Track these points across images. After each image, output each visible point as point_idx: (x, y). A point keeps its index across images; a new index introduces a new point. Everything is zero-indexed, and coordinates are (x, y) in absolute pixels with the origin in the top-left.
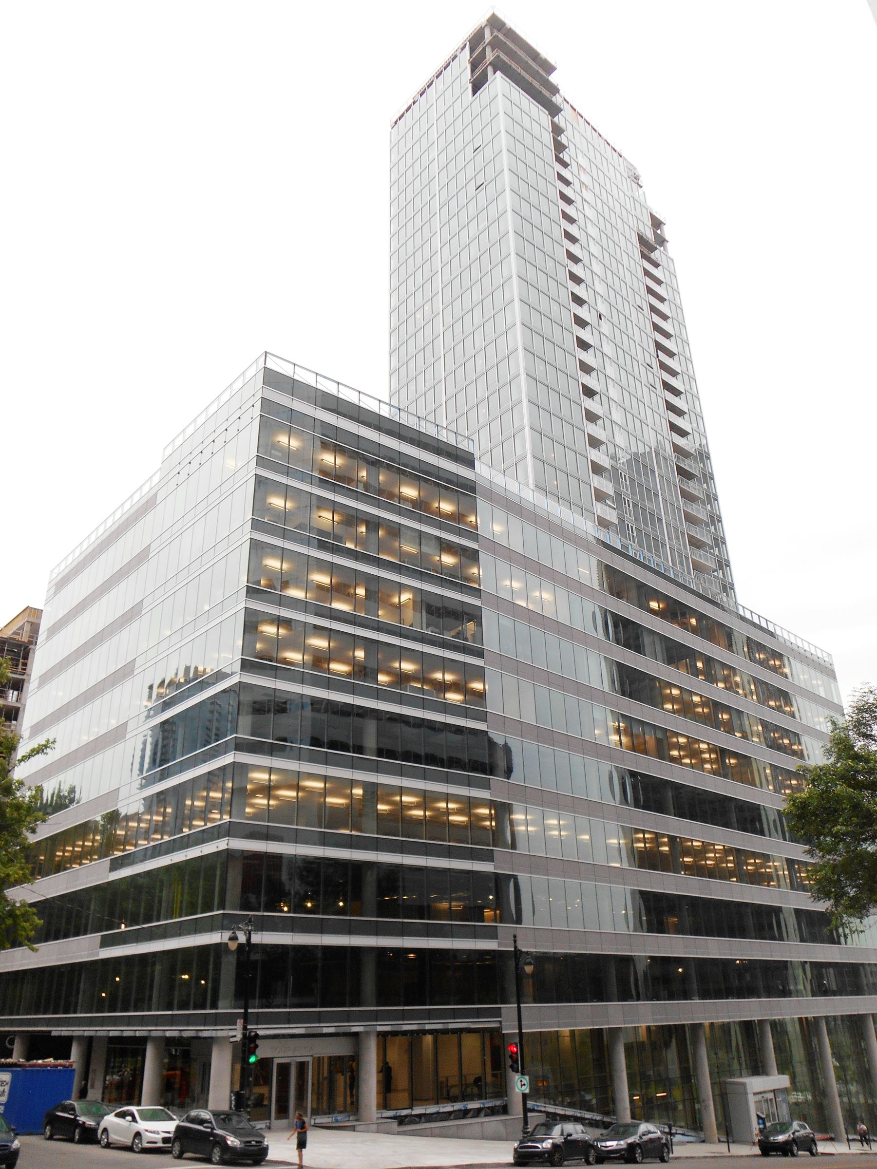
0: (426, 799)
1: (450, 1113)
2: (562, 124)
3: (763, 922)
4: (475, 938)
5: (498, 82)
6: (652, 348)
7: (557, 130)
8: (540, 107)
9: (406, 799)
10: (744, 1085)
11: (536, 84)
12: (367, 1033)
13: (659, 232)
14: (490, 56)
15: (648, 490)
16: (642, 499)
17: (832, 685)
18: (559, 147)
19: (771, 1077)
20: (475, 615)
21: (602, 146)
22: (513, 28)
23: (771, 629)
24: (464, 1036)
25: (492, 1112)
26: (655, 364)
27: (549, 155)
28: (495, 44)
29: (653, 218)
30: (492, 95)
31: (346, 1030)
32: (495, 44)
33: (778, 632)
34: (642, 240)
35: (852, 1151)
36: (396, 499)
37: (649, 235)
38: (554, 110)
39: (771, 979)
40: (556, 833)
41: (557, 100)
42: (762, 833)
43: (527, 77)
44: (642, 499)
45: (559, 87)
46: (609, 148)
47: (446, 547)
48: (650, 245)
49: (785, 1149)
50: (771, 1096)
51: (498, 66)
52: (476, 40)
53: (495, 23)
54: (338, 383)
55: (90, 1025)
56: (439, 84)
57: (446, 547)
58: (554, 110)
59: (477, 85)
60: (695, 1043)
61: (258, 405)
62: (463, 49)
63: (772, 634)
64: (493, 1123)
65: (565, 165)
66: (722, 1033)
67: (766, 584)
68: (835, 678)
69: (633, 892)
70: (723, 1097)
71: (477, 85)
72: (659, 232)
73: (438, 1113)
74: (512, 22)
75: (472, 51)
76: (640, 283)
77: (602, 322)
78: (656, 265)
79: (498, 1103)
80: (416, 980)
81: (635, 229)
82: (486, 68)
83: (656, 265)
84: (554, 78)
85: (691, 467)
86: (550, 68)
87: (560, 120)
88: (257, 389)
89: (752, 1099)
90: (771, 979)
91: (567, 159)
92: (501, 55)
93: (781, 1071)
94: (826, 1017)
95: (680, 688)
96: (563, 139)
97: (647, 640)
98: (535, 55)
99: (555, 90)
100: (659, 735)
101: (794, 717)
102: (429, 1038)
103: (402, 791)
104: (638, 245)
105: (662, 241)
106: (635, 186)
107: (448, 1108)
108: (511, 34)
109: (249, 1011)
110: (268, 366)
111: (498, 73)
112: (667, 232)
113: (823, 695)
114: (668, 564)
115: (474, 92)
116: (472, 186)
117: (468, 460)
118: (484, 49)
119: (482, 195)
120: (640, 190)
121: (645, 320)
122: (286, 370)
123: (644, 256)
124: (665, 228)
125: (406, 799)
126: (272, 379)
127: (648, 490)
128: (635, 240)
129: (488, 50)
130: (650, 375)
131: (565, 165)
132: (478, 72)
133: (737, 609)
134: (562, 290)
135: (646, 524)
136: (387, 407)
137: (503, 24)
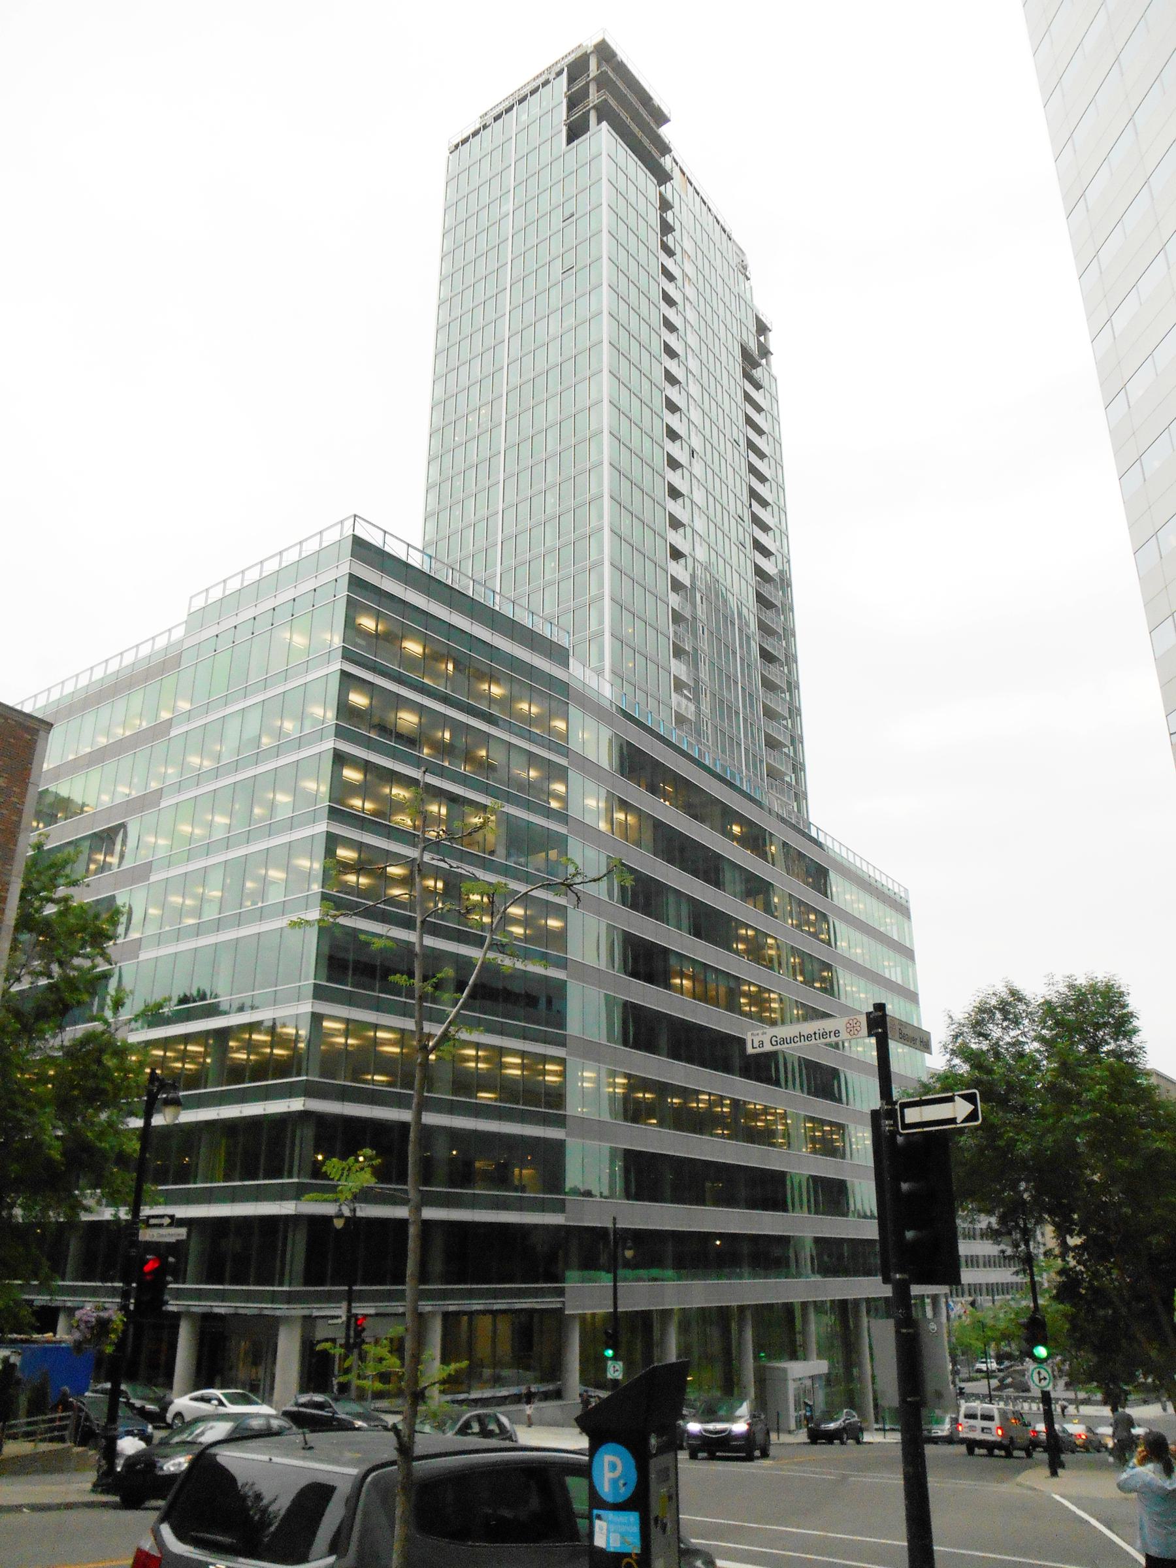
0: (352, 1027)
1: (506, 1397)
2: (669, 196)
3: (767, 1190)
4: (543, 1211)
5: (602, 136)
6: (745, 496)
7: (665, 205)
8: (629, 152)
9: (380, 1034)
10: (785, 1370)
11: (646, 142)
12: (433, 1313)
13: (762, 339)
14: (594, 97)
15: (728, 677)
16: (721, 688)
17: (906, 926)
18: (666, 228)
19: (811, 1363)
20: (560, 842)
21: (711, 222)
22: (625, 61)
23: (821, 839)
24: (500, 1317)
25: (546, 1396)
26: (747, 517)
27: (654, 241)
28: (602, 82)
29: (759, 321)
30: (594, 151)
31: (490, 1307)
32: (602, 82)
33: (828, 843)
34: (745, 353)
35: (887, 1440)
36: (486, 703)
37: (753, 346)
38: (662, 177)
39: (768, 1255)
40: (472, 1065)
41: (666, 162)
42: (777, 1083)
43: (636, 130)
44: (721, 688)
45: (671, 146)
46: (718, 228)
47: (532, 759)
48: (753, 360)
49: (830, 1437)
50: (808, 1383)
51: (604, 113)
52: (577, 69)
53: (604, 51)
54: (409, 545)
55: (247, 1301)
56: (521, 114)
57: (532, 759)
58: (662, 177)
59: (575, 131)
60: (857, 1317)
61: (345, 581)
62: (559, 74)
63: (816, 842)
64: (550, 1407)
65: (670, 253)
66: (762, 1313)
67: (849, 800)
68: (909, 918)
69: (613, 1151)
70: (761, 1380)
71: (575, 131)
72: (762, 339)
73: (494, 1398)
74: (626, 53)
75: (571, 80)
76: (737, 410)
77: (694, 461)
78: (758, 387)
79: (551, 1387)
80: (475, 1255)
81: (739, 338)
82: (589, 111)
83: (758, 387)
84: (665, 131)
85: (774, 648)
86: (661, 118)
87: (668, 190)
88: (346, 566)
89: (792, 1387)
90: (768, 1255)
91: (671, 243)
92: (605, 97)
93: (820, 1356)
94: (868, 1300)
95: (755, 929)
96: (669, 216)
97: (728, 875)
98: (646, 99)
99: (665, 149)
100: (732, 984)
101: (829, 944)
102: (466, 1318)
103: (376, 1027)
104: (740, 360)
105: (765, 352)
106: (741, 277)
107: (504, 1392)
108: (621, 69)
109: (355, 1288)
110: (356, 533)
111: (604, 123)
112: (774, 341)
113: (896, 938)
114: (712, 753)
115: (570, 140)
116: (557, 267)
117: (559, 654)
118: (588, 84)
119: (570, 282)
120: (747, 283)
121: (738, 459)
122: (375, 539)
123: (747, 376)
124: (771, 335)
125: (380, 1034)
126: (361, 548)
127: (728, 677)
128: (737, 352)
129: (592, 88)
130: (741, 529)
131: (670, 253)
132: (578, 113)
133: (809, 829)
134: (656, 420)
135: (722, 719)
136: (420, 554)
137: (614, 55)
